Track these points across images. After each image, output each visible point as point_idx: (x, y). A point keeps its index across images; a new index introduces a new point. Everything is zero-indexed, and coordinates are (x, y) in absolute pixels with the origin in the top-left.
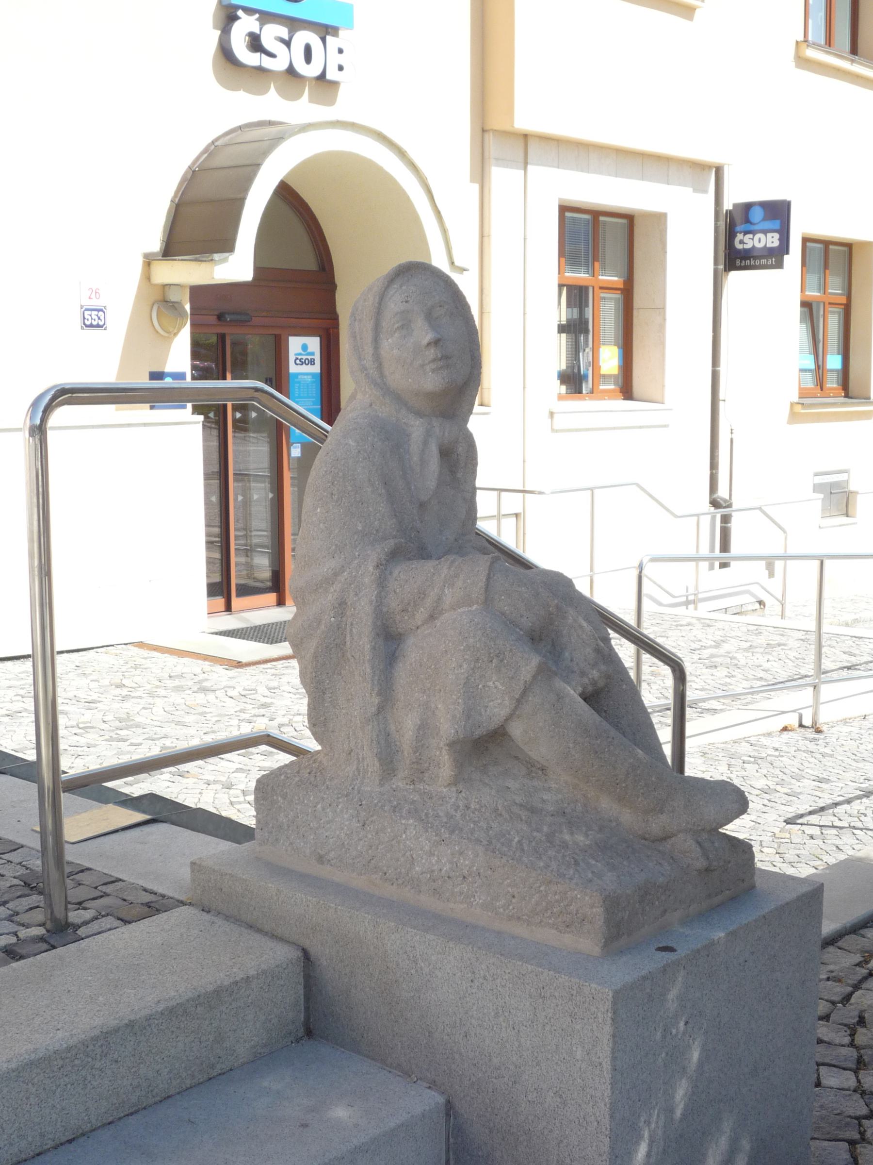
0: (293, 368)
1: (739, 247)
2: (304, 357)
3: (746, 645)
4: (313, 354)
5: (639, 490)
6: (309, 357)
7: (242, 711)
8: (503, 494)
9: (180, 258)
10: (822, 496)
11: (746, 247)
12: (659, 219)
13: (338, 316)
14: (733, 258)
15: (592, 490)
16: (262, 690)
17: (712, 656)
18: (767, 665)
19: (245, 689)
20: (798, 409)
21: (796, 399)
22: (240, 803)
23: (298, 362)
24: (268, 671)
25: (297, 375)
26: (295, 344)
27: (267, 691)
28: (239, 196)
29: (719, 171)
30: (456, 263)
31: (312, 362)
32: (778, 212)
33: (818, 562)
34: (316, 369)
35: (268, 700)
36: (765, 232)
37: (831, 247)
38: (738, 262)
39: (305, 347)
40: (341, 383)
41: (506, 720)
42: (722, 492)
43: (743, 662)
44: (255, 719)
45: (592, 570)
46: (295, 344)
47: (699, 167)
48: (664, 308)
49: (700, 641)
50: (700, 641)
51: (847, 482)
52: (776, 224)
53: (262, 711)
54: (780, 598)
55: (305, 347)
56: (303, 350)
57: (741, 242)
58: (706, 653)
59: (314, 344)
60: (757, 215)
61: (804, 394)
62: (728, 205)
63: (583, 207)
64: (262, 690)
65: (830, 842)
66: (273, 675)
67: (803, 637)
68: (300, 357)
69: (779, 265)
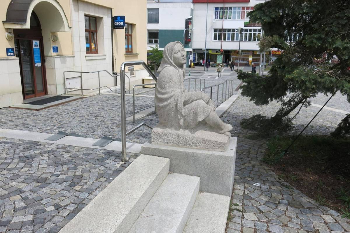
0: (34, 47)
4: (37, 44)
5: (106, 72)
8: (82, 73)
9: (12, 23)
11: (117, 24)
12: (102, 18)
14: (114, 27)
15: (99, 72)
20: (126, 55)
21: (125, 53)
25: (35, 48)
26: (34, 42)
29: (111, 9)
30: (105, 71)
31: (38, 46)
32: (123, 18)
33: (98, 72)
34: (39, 47)
36: (121, 22)
37: (91, 18)
38: (115, 28)
39: (36, 43)
41: (329, 223)
42: (115, 71)
45: (99, 87)
46: (34, 42)
47: (107, 8)
48: (103, 36)
51: (134, 69)
52: (123, 20)
54: (128, 90)
55: (36, 43)
56: (35, 43)
57: (116, 23)
59: (38, 42)
60: (119, 18)
61: (126, 52)
62: (113, 16)
63: (88, 15)
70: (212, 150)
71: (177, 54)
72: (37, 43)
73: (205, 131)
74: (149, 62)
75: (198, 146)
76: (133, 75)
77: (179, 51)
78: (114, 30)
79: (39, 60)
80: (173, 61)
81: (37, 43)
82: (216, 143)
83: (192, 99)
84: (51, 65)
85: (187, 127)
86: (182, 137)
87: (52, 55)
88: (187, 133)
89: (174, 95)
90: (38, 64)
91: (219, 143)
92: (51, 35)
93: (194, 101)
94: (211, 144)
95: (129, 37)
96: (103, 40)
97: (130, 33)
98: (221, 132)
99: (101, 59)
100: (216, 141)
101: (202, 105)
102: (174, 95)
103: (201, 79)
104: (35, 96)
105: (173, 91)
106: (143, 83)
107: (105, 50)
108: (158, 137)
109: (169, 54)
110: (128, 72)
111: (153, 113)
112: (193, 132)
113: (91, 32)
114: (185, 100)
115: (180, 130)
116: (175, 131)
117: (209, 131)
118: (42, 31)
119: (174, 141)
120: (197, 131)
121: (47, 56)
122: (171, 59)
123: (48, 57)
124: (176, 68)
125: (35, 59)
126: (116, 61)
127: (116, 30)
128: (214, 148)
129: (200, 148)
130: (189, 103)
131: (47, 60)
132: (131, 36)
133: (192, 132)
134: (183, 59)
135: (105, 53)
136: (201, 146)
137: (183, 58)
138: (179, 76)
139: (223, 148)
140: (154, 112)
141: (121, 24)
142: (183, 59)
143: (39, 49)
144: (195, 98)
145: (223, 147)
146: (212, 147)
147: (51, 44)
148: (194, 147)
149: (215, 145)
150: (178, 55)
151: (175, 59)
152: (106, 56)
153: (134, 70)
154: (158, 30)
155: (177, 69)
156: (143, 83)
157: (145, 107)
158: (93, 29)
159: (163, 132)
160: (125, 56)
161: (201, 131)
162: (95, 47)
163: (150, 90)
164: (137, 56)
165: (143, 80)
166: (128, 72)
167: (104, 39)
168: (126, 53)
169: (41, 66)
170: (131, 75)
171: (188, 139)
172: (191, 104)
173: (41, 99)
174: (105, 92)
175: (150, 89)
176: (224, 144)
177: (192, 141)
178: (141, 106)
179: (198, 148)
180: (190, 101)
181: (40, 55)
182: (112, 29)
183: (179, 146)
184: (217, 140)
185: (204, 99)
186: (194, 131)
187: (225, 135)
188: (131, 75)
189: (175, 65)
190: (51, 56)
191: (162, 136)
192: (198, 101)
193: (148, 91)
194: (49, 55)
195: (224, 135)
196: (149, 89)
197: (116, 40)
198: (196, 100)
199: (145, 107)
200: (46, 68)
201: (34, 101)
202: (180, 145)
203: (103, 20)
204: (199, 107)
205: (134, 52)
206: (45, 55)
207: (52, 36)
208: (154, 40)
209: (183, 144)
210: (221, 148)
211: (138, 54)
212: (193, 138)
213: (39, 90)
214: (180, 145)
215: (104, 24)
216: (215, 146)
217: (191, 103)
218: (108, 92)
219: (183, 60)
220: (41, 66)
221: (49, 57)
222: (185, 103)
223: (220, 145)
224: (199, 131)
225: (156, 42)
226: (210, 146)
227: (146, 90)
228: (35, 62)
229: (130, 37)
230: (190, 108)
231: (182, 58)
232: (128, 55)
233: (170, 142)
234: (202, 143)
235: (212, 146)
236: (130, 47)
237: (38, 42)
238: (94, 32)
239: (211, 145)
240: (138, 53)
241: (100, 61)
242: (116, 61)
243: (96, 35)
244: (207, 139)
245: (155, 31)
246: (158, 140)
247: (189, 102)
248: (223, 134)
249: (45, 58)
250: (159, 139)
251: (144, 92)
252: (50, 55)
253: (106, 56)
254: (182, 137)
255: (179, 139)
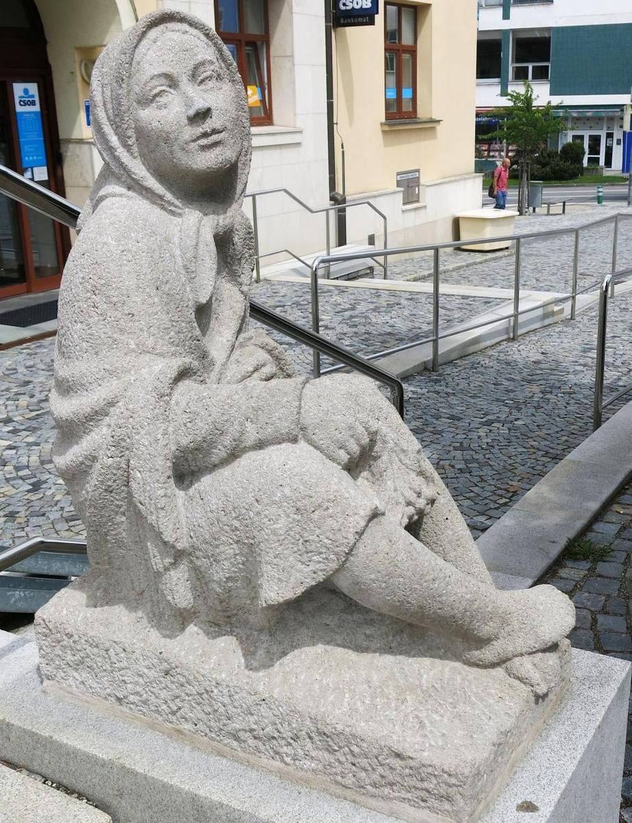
0: (19, 109)
1: (343, 8)
2: (27, 99)
3: (372, 306)
4: (33, 96)
6: (31, 99)
7: (8, 390)
10: (402, 189)
13: (24, 327)
16: (21, 369)
17: (352, 317)
18: (391, 322)
19: (8, 369)
20: (387, 128)
21: (383, 120)
22: (14, 479)
23: (22, 103)
24: (24, 351)
26: (18, 89)
27: (25, 370)
28: (54, 299)
30: (283, 192)
31: (33, 103)
34: (37, 108)
35: (27, 379)
38: (342, 21)
39: (26, 91)
40: (57, 107)
42: (339, 190)
43: (374, 320)
44: (18, 397)
46: (18, 89)
49: (340, 305)
50: (340, 305)
51: (418, 178)
53: (22, 390)
55: (26, 91)
56: (24, 93)
58: (348, 314)
59: (33, 88)
61: (389, 116)
64: (21, 369)
65: (475, 474)
66: (28, 354)
67: (410, 297)
68: (23, 99)
69: (372, 22)
70: (373, 802)
71: (159, 108)
72: (30, 94)
73: (352, 655)
74: (512, 151)
75: (288, 760)
76: (418, 201)
77: (172, 82)
78: (340, 29)
79: (42, 157)
80: (142, 155)
81: (30, 94)
82: (396, 763)
83: (227, 440)
84: (81, 175)
85: (225, 613)
86: (189, 682)
87: (84, 137)
88: (213, 657)
89: (112, 404)
90: (35, 169)
91: (420, 772)
92: (77, 57)
93: (245, 450)
94: (364, 762)
95: (401, 59)
96: (292, 70)
97: (407, 39)
98: (476, 653)
99: (280, 146)
100: (398, 748)
101: (287, 491)
102: (112, 404)
103: (576, 231)
104: (29, 291)
105: (112, 373)
106: (457, 236)
107: (298, 111)
108: (69, 658)
109: (109, 106)
110: (395, 193)
111: (426, 369)
112: (261, 653)
113: (243, 43)
114: (184, 441)
115: (183, 629)
116: (154, 635)
117: (389, 650)
118: (49, 49)
119: (153, 698)
120: (293, 647)
121: (69, 141)
122: (127, 147)
123: (71, 146)
124: (163, 208)
125: (23, 154)
126: (343, 152)
127: (347, 29)
128: (387, 790)
129: (301, 774)
130: (215, 467)
131: (69, 154)
132: (413, 51)
133: (254, 653)
134: (204, 142)
135: (299, 125)
136: (308, 764)
137: (199, 130)
138: (179, 261)
139: (447, 806)
140: (430, 366)
141: (364, 7)
142: (204, 142)
143: (39, 116)
144: (252, 435)
145: (449, 799)
146: (374, 785)
147: (81, 95)
148: (264, 761)
149: (391, 777)
150: (164, 112)
151: (150, 144)
152: (301, 132)
153: (418, 186)
154: (549, 29)
155: (172, 213)
156: (457, 236)
157: (401, 340)
158: (253, 29)
159: (91, 633)
160: (384, 132)
161: (320, 648)
162: (263, 101)
163: (478, 260)
164: (433, 128)
165: (456, 222)
166: (395, 193)
167: (296, 67)
168: (386, 120)
169: (47, 179)
170: (404, 204)
171: (226, 700)
172: (225, 472)
173: (33, 303)
174: (283, 274)
175: (479, 257)
176: (453, 781)
177: (252, 719)
178: (390, 334)
179: (291, 768)
180: (219, 453)
181: (42, 139)
182: (327, 27)
183: (179, 731)
184: (409, 742)
185: (320, 437)
186: (275, 648)
187: (509, 673)
188: (404, 204)
189: (152, 183)
190: (81, 142)
191: (88, 656)
192: (272, 451)
193: (468, 266)
194: (74, 137)
195: (499, 672)
196: (478, 255)
197: (347, 70)
198: (260, 445)
199: (401, 340)
200: (66, 184)
201: (12, 309)
202: (186, 726)
203: (430, 13)
204: (266, 500)
205: (422, 113)
206: (62, 136)
207: (81, 62)
208: (533, 67)
209: (201, 726)
210: (432, 802)
211: (439, 121)
212: (250, 700)
213: (49, 266)
214: (186, 726)
215: (295, 9)
216: (392, 784)
217: (225, 462)
218: (296, 271)
219: (204, 148)
220: (47, 179)
221: (74, 145)
222: (187, 469)
223: (425, 785)
224: (307, 649)
225: (541, 74)
226: (363, 774)
227: (465, 258)
228: (25, 166)
229: (406, 56)
230: (215, 502)
231: (189, 132)
232: (395, 125)
233: (132, 698)
234: (309, 746)
235: (376, 777)
236: (407, 94)
237: (33, 88)
238: (259, 43)
239: (365, 770)
240: (435, 117)
241: (275, 153)
242: (343, 152)
243: (265, 51)
244: (340, 727)
245: (538, 35)
246: (68, 670)
247: (215, 459)
248: (493, 665)
249: (63, 149)
250: (76, 670)
251: (454, 270)
252: (76, 135)
253: (301, 132)
254: (189, 682)
255: (177, 692)
